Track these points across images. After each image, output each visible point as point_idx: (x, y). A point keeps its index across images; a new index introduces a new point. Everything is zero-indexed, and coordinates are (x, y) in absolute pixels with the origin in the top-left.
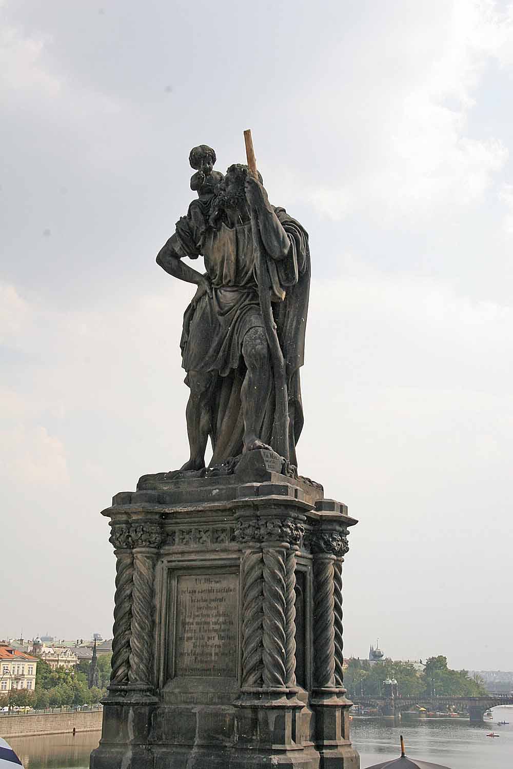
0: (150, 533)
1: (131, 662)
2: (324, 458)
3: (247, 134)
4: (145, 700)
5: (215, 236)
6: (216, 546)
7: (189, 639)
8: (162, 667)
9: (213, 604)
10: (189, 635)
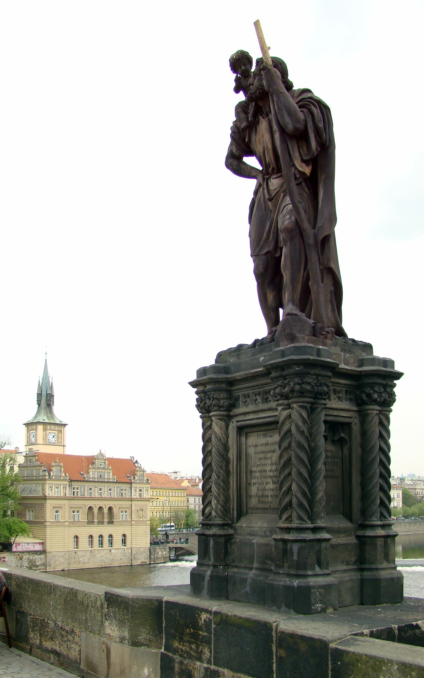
0: (219, 400)
2: (363, 317)
3: (257, 24)
4: (221, 532)
5: (256, 131)
6: (265, 406)
7: (255, 484)
8: (235, 507)
9: (269, 455)
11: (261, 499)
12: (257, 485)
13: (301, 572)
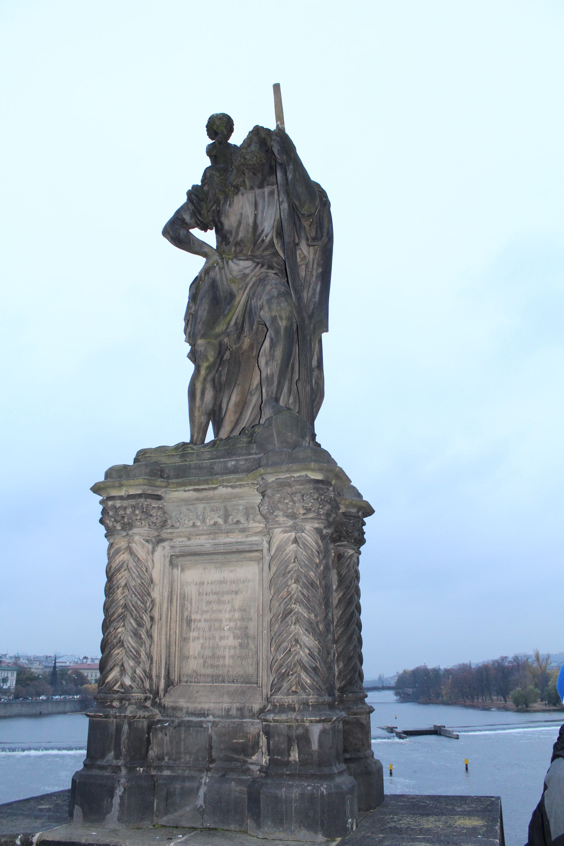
1: (126, 665)
3: (277, 88)
9: (226, 598)
11: (209, 662)
12: (201, 641)
13: (326, 770)
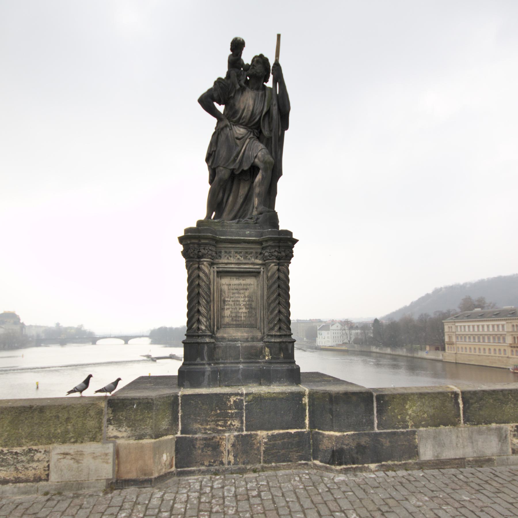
3: (279, 36)
9: (242, 291)
10: (228, 307)
